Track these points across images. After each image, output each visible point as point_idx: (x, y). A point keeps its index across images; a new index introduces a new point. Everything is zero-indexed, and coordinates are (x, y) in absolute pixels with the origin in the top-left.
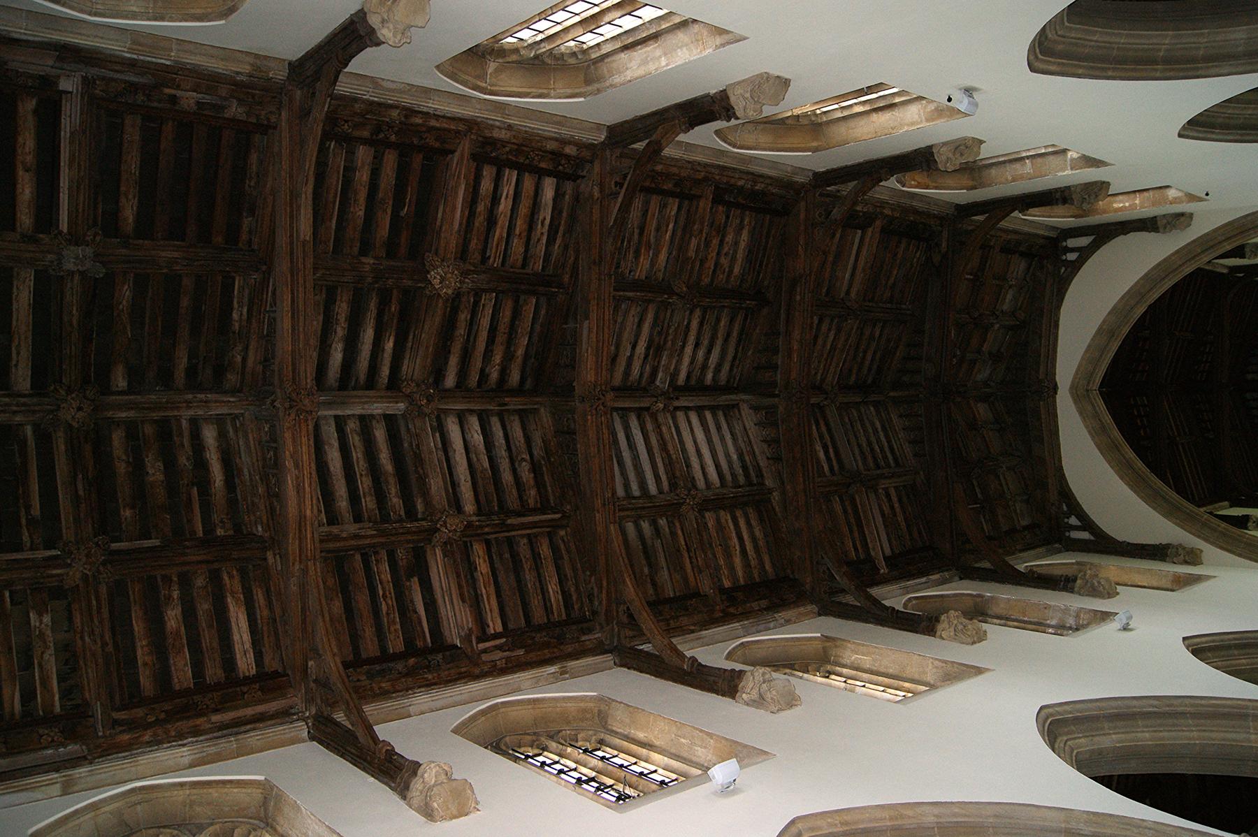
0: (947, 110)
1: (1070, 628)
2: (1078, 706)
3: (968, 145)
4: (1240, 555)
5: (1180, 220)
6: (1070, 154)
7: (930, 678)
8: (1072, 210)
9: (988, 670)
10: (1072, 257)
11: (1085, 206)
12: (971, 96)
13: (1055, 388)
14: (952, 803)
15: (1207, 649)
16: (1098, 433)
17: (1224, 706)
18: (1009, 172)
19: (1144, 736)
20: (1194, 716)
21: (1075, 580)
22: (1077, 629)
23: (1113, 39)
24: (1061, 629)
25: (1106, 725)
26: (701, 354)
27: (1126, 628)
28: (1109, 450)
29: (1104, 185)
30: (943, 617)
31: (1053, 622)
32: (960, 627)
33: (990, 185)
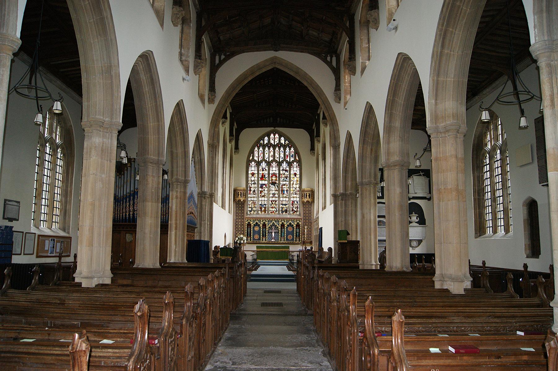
0: (391, 18)
1: (181, 58)
2: (154, 64)
3: (376, 24)
4: (213, 117)
5: (338, 99)
6: (368, 62)
7: (156, 4)
8: (347, 60)
9: (163, 29)
10: (329, 59)
11: (347, 66)
12: (394, 29)
13: (276, 51)
14: (114, 27)
15: (179, 108)
16: (258, 67)
17: (161, 115)
18: (364, 38)
19: (146, 89)
20: (156, 105)
21: (200, 59)
22: (181, 60)
23: (404, 83)
24: (181, 54)
25: (149, 75)
26: (249, 231)
27: (184, 79)
28: (251, 70)
29: (354, 74)
30: (182, 9)
31: (182, 51)
32: (178, 16)
33: (360, 29)
